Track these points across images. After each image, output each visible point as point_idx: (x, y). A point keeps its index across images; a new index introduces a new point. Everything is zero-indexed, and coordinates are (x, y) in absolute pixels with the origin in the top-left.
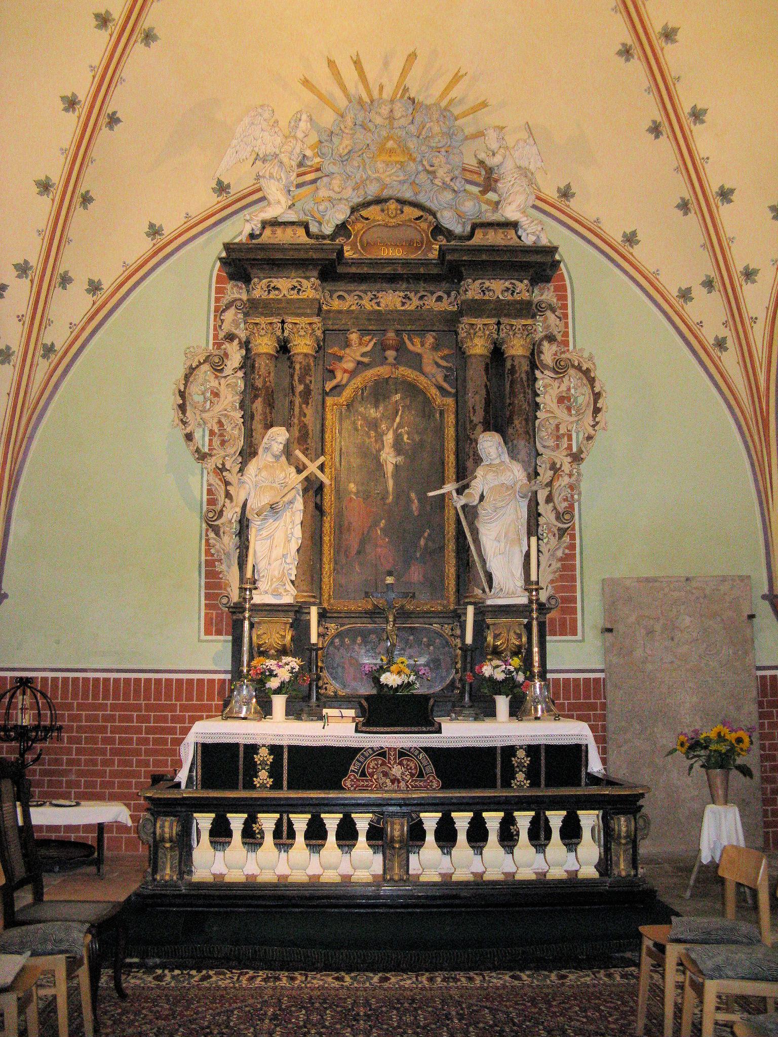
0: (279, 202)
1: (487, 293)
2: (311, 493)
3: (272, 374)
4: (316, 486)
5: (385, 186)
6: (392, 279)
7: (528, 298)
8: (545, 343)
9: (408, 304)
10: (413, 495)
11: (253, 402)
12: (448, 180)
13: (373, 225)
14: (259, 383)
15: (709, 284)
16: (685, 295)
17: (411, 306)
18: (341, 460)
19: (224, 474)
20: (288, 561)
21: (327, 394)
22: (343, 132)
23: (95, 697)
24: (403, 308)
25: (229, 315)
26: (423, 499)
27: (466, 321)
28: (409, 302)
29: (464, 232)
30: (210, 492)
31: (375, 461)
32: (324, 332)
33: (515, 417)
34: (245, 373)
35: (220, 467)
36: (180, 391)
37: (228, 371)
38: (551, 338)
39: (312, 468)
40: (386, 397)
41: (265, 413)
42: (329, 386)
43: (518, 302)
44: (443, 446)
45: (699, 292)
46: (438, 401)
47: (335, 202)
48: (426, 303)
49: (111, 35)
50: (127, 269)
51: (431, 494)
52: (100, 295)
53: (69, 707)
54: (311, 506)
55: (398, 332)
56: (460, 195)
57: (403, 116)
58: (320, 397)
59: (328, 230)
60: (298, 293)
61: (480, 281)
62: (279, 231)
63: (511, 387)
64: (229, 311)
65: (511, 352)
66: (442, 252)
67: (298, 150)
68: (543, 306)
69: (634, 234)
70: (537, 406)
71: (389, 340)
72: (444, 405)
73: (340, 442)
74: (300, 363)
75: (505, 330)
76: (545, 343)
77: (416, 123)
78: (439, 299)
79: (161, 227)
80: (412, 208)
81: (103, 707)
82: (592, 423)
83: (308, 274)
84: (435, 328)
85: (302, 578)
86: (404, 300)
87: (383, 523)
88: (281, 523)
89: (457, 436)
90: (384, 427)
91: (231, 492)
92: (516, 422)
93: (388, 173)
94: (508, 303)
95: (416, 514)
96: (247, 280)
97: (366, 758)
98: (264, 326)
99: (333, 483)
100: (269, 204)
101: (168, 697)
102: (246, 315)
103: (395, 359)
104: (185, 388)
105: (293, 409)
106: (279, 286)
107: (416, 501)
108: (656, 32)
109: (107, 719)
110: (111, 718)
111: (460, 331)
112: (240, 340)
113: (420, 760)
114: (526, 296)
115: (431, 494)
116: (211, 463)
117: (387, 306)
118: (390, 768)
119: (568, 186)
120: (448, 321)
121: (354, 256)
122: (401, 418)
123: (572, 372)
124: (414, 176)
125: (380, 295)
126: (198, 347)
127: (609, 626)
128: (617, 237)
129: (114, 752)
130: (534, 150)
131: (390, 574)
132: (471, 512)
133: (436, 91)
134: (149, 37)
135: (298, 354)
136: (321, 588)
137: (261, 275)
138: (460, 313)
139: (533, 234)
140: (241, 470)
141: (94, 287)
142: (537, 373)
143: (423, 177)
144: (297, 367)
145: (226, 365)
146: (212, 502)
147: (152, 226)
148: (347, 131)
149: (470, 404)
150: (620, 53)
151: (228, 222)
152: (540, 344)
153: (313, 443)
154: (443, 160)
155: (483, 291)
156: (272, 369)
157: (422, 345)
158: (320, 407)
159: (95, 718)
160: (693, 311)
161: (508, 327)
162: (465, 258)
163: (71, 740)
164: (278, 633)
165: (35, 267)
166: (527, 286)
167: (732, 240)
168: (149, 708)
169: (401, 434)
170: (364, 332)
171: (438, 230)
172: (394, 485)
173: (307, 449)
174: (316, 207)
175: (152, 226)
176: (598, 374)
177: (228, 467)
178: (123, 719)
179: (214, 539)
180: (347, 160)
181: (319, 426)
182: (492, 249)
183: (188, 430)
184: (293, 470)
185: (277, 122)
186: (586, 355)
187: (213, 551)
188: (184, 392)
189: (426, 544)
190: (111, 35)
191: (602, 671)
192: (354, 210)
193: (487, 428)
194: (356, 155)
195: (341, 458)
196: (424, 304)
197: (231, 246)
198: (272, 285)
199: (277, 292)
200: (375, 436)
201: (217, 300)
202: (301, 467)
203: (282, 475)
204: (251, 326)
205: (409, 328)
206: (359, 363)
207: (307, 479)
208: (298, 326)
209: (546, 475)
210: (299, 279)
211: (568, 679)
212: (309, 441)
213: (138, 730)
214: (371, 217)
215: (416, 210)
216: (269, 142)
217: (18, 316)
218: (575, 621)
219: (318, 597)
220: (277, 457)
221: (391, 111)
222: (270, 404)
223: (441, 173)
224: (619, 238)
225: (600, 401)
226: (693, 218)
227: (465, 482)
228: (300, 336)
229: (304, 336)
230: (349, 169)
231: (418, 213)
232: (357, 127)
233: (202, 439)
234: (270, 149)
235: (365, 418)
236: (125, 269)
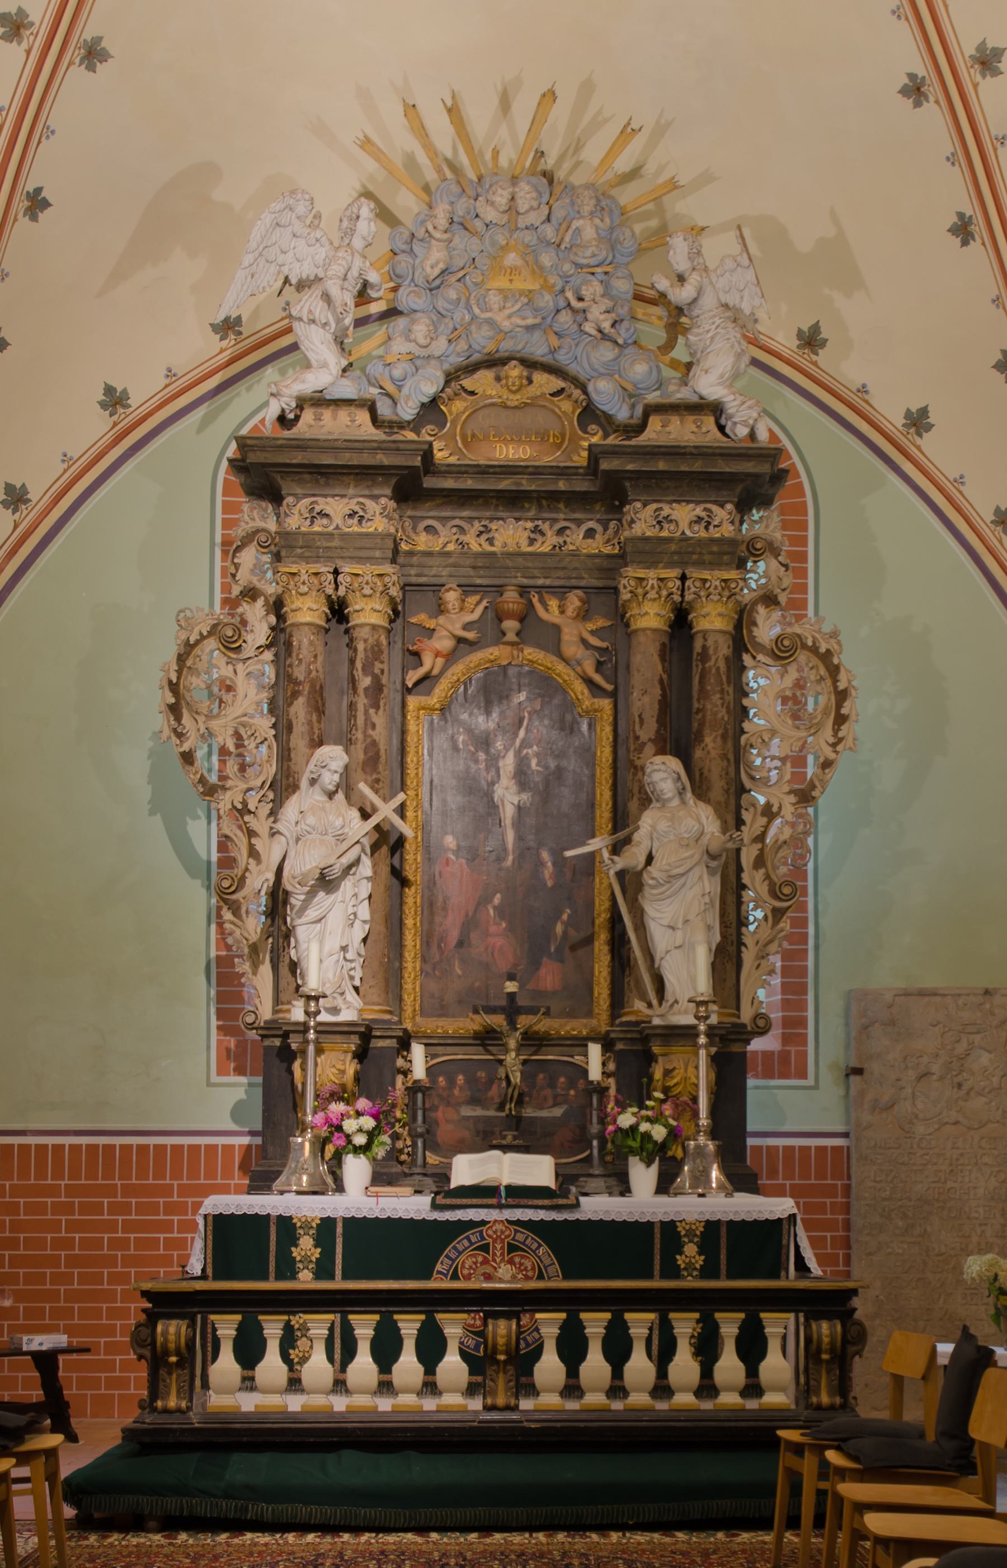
0: (325, 365)
1: (666, 525)
2: (384, 850)
3: (320, 659)
5: (503, 334)
7: (732, 535)
8: (761, 609)
9: (540, 542)
10: (545, 855)
11: (290, 704)
12: (606, 326)
13: (482, 404)
17: (544, 546)
18: (431, 800)
19: (247, 818)
21: (410, 691)
22: (430, 236)
23: (92, 1175)
24: (530, 549)
25: (248, 557)
26: (560, 862)
28: (540, 539)
29: (632, 417)
30: (222, 847)
31: (485, 799)
32: (402, 588)
33: (707, 731)
34: (275, 655)
35: (239, 806)
36: (170, 682)
37: (249, 651)
38: (770, 600)
39: (386, 811)
40: (504, 697)
41: (310, 723)
43: (713, 540)
48: (568, 540)
49: (28, 52)
50: (69, 467)
51: (569, 854)
52: (25, 512)
54: (385, 870)
55: (524, 591)
56: (627, 351)
57: (532, 208)
58: (398, 697)
59: (408, 411)
60: (360, 522)
61: (655, 506)
62: (327, 414)
63: (701, 682)
64: (247, 549)
65: (701, 624)
66: (595, 454)
68: (758, 546)
69: (924, 412)
70: (745, 711)
71: (508, 602)
72: (596, 711)
73: (431, 769)
74: (365, 641)
75: (693, 589)
76: (761, 609)
77: (553, 219)
78: (590, 533)
79: (125, 391)
80: (546, 376)
81: (53, 1191)
82: (831, 740)
83: (376, 492)
84: (583, 583)
85: (372, 984)
86: (532, 536)
87: (497, 899)
88: (338, 895)
89: (615, 760)
90: (499, 745)
91: (257, 847)
92: (708, 740)
93: (507, 312)
94: (700, 542)
96: (276, 498)
97: (460, 1253)
99: (419, 834)
100: (308, 365)
102: (277, 557)
103: (518, 634)
104: (179, 678)
105: (355, 717)
106: (328, 510)
107: (549, 864)
108: (967, 55)
109: (58, 1208)
110: (68, 1208)
111: (621, 587)
113: (539, 1257)
114: (727, 530)
115: (569, 854)
116: (225, 801)
118: (495, 1268)
119: (816, 328)
120: (601, 569)
121: (453, 460)
122: (527, 730)
123: (802, 656)
124: (549, 319)
125: (493, 526)
126: (199, 609)
127: (854, 1063)
128: (895, 418)
129: (73, 1261)
130: (750, 275)
131: (511, 977)
133: (593, 153)
136: (401, 999)
138: (622, 558)
139: (745, 423)
140: (273, 813)
142: (747, 659)
143: (565, 318)
144: (361, 646)
145: (244, 641)
147: (109, 390)
150: (905, 91)
151: (241, 386)
153: (386, 770)
154: (599, 289)
155: (659, 522)
156: (320, 649)
157: (562, 612)
158: (397, 711)
159: (41, 1208)
161: (698, 584)
162: (630, 467)
164: (334, 1066)
166: (730, 513)
168: (128, 1191)
170: (467, 589)
172: (515, 839)
173: (377, 781)
174: (387, 374)
175: (109, 390)
176: (845, 659)
177: (252, 807)
179: (233, 923)
180: (438, 287)
181: (396, 742)
183: (186, 747)
184: (355, 814)
185: (318, 216)
186: (827, 628)
188: (177, 684)
189: (565, 933)
190: (28, 52)
191: (846, 1135)
192: (450, 377)
193: (661, 751)
194: (453, 279)
195: (431, 795)
196: (565, 542)
197: (249, 442)
198: (318, 509)
199: (325, 521)
200: (486, 760)
201: (227, 524)
202: (369, 810)
203: (339, 822)
204: (285, 578)
205: (540, 582)
206: (460, 640)
207: (377, 828)
208: (360, 579)
210: (361, 500)
211: (792, 1148)
212: (381, 768)
213: (112, 1226)
214: (479, 390)
215: (552, 378)
219: (397, 1012)
220: (331, 795)
221: (513, 199)
222: (318, 707)
223: (596, 313)
224: (899, 421)
225: (847, 704)
228: (365, 596)
229: (370, 596)
230: (441, 304)
231: (558, 384)
232: (455, 226)
233: (208, 764)
234: (306, 270)
235: (469, 731)
236: (65, 466)
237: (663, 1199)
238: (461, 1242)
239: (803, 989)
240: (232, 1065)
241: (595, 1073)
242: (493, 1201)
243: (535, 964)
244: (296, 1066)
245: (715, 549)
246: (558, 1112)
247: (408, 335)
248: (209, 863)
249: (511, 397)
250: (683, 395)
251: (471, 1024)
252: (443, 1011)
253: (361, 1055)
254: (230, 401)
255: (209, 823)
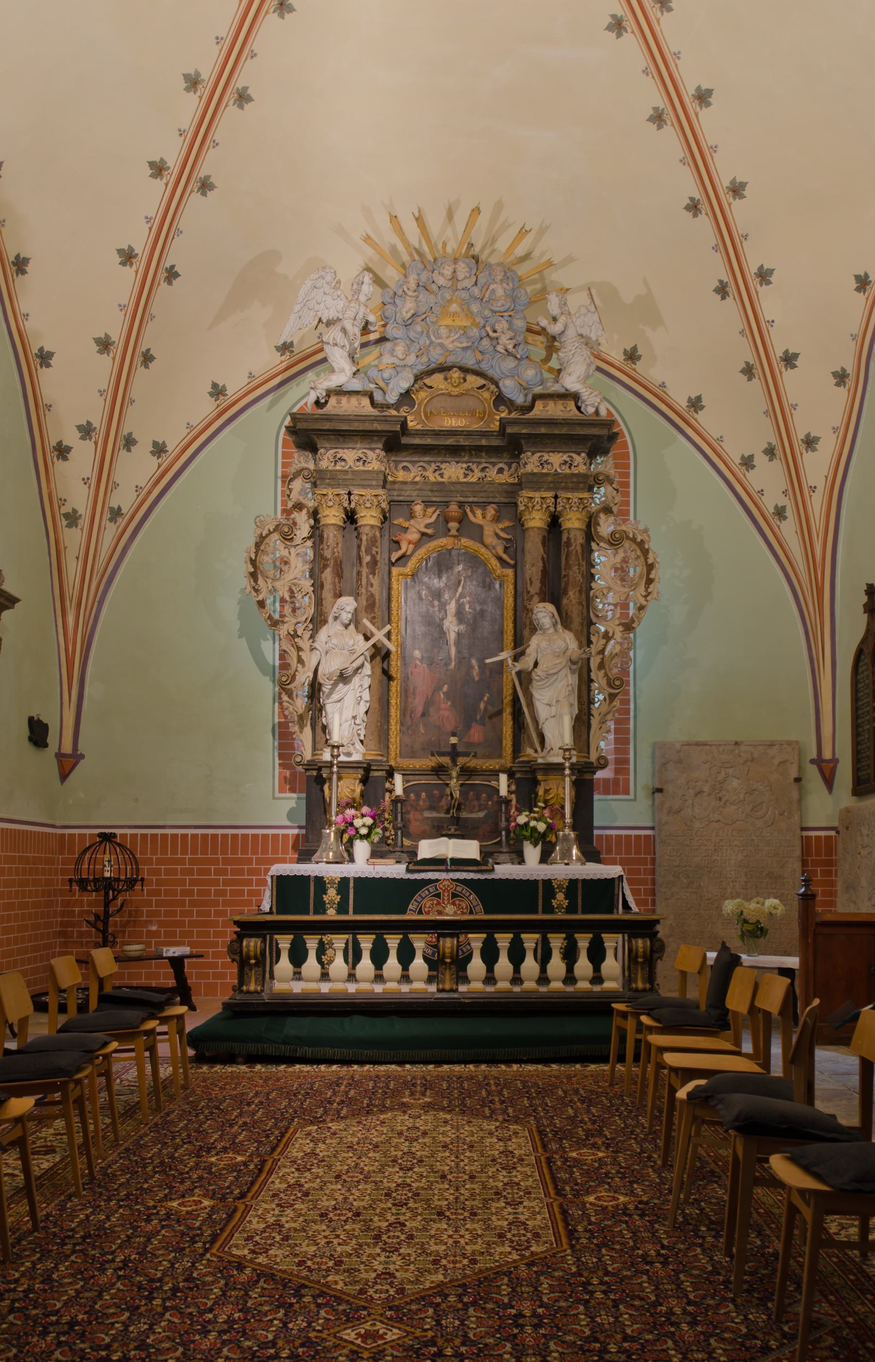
0: (343, 371)
1: (545, 466)
2: (378, 659)
3: (340, 545)
4: (383, 652)
6: (455, 451)
8: (602, 516)
10: (474, 662)
12: (510, 347)
14: (328, 554)
15: (770, 452)
16: (748, 462)
19: (296, 640)
20: (357, 722)
21: (393, 564)
22: (406, 294)
23: (174, 852)
24: (465, 480)
25: (298, 485)
27: (525, 495)
28: (471, 474)
33: (570, 588)
34: (314, 543)
35: (292, 633)
36: (251, 559)
37: (298, 540)
39: (379, 636)
40: (449, 568)
41: (334, 583)
42: (395, 556)
43: (573, 475)
44: (502, 615)
45: (761, 460)
46: (499, 572)
47: (398, 369)
48: (488, 475)
49: (167, 185)
51: (488, 661)
53: (149, 861)
54: (379, 671)
55: (461, 505)
57: (466, 277)
58: (387, 568)
59: (392, 398)
61: (539, 454)
62: (344, 400)
66: (503, 424)
67: (361, 315)
68: (601, 478)
73: (406, 611)
74: (367, 535)
76: (602, 516)
77: (479, 283)
78: (500, 471)
79: (224, 386)
80: (474, 377)
81: (182, 861)
82: (644, 594)
83: (373, 446)
84: (496, 500)
87: (445, 688)
88: (351, 686)
89: (515, 606)
90: (446, 596)
92: (571, 593)
93: (451, 339)
95: (476, 679)
97: (423, 898)
98: (331, 497)
100: (333, 371)
101: (245, 851)
102: (315, 485)
103: (458, 531)
104: (256, 557)
106: (345, 457)
109: (185, 872)
110: (190, 872)
111: (519, 503)
112: (308, 510)
114: (582, 469)
115: (488, 661)
116: (284, 630)
117: (450, 477)
120: (507, 492)
124: (476, 344)
125: (443, 466)
129: (193, 903)
130: (595, 317)
131: (454, 734)
132: (525, 678)
133: (502, 245)
134: (205, 186)
135: (365, 525)
136: (388, 748)
137: (328, 445)
140: (312, 637)
141: (159, 449)
142: (594, 545)
144: (364, 538)
146: (285, 666)
148: (410, 293)
149: (528, 577)
151: (293, 383)
152: (597, 516)
155: (542, 464)
156: (340, 539)
157: (484, 518)
158: (386, 576)
160: (755, 479)
161: (565, 501)
162: (524, 431)
163: (151, 893)
165: (98, 428)
167: (794, 407)
168: (226, 861)
169: (463, 604)
170: (427, 504)
171: (500, 400)
173: (374, 618)
177: (299, 633)
178: (201, 872)
179: (288, 702)
181: (385, 595)
182: (550, 422)
183: (260, 598)
184: (361, 637)
185: (339, 282)
186: (641, 527)
187: (286, 713)
188: (255, 560)
189: (486, 708)
190: (167, 185)
191: (653, 828)
192: (417, 378)
193: (543, 600)
194: (419, 319)
197: (298, 416)
198: (339, 456)
199: (343, 463)
202: (369, 635)
204: (319, 497)
205: (471, 500)
206: (423, 534)
207: (374, 646)
208: (364, 498)
209: (597, 643)
210: (364, 451)
211: (621, 836)
213: (216, 883)
214: (435, 386)
215: (478, 378)
216: (330, 308)
217: (83, 479)
218: (627, 781)
220: (346, 626)
221: (455, 272)
222: (339, 574)
224: (684, 404)
225: (653, 572)
226: (756, 384)
227: (519, 650)
230: (412, 334)
231: (481, 381)
232: (420, 288)
233: (274, 608)
234: (332, 314)
235: (429, 588)
236: (189, 430)
237: (544, 866)
238: (424, 892)
239: (627, 741)
240: (288, 787)
241: (503, 791)
242: (443, 868)
243: (468, 727)
244: (326, 787)
245: (575, 480)
246: (481, 815)
247: (392, 353)
248: (274, 666)
249: (454, 389)
250: (556, 388)
251: (430, 762)
252: (413, 755)
253: (364, 781)
254: (286, 392)
255: (274, 643)
